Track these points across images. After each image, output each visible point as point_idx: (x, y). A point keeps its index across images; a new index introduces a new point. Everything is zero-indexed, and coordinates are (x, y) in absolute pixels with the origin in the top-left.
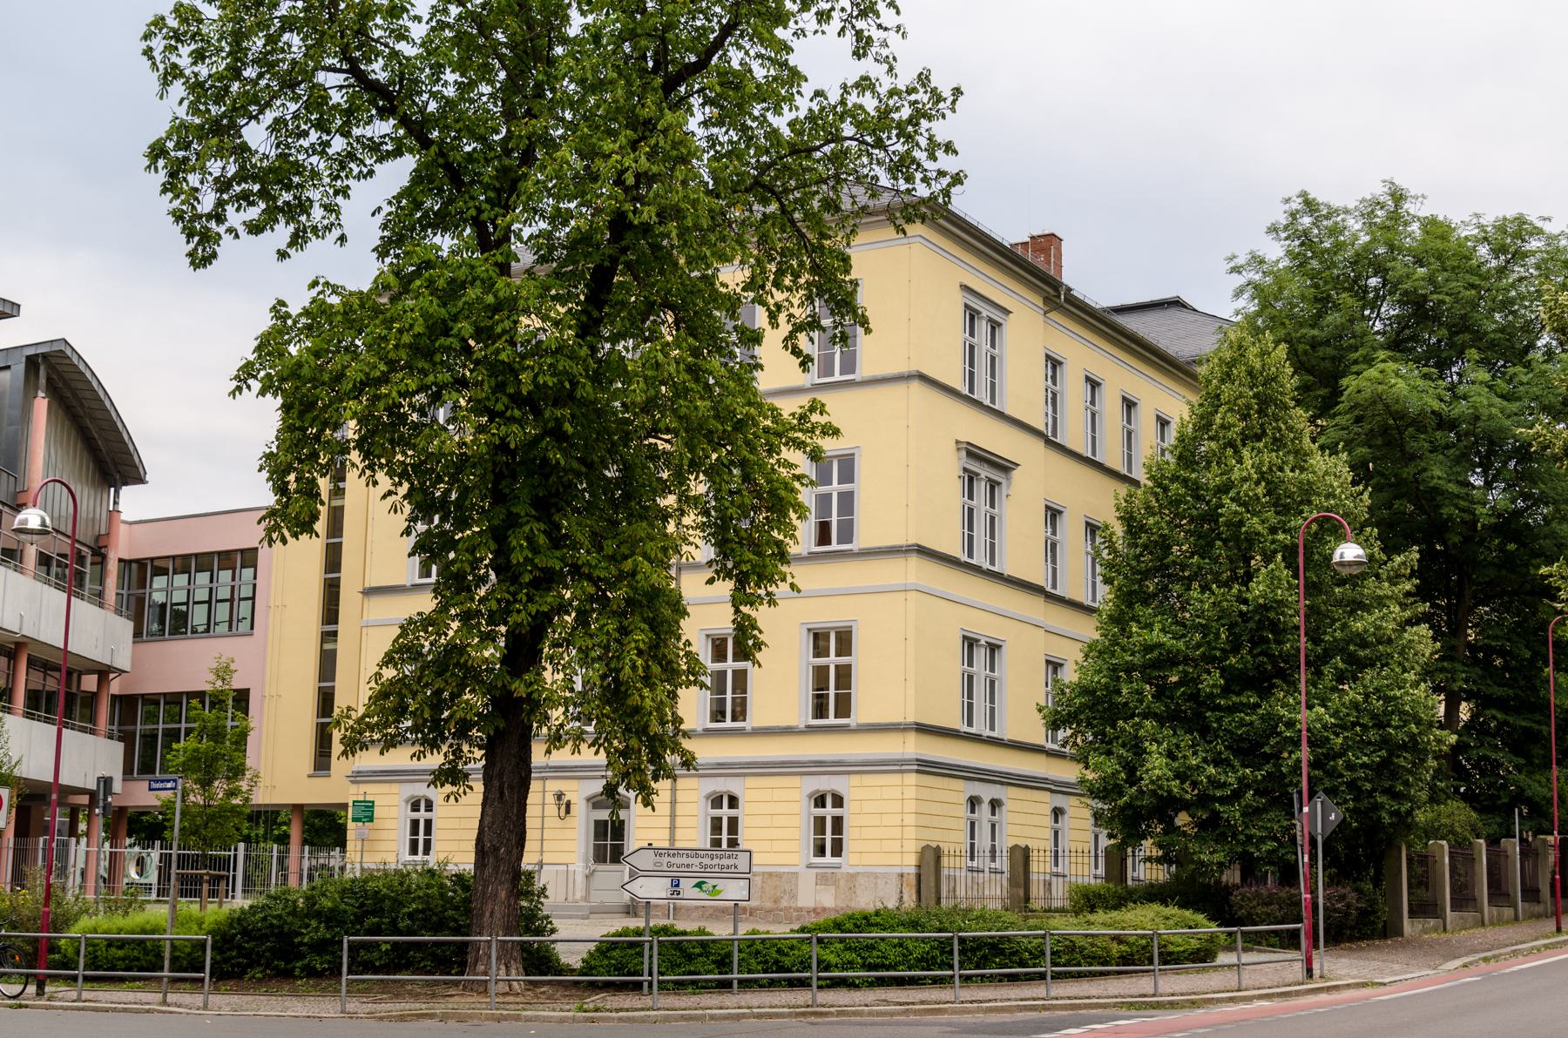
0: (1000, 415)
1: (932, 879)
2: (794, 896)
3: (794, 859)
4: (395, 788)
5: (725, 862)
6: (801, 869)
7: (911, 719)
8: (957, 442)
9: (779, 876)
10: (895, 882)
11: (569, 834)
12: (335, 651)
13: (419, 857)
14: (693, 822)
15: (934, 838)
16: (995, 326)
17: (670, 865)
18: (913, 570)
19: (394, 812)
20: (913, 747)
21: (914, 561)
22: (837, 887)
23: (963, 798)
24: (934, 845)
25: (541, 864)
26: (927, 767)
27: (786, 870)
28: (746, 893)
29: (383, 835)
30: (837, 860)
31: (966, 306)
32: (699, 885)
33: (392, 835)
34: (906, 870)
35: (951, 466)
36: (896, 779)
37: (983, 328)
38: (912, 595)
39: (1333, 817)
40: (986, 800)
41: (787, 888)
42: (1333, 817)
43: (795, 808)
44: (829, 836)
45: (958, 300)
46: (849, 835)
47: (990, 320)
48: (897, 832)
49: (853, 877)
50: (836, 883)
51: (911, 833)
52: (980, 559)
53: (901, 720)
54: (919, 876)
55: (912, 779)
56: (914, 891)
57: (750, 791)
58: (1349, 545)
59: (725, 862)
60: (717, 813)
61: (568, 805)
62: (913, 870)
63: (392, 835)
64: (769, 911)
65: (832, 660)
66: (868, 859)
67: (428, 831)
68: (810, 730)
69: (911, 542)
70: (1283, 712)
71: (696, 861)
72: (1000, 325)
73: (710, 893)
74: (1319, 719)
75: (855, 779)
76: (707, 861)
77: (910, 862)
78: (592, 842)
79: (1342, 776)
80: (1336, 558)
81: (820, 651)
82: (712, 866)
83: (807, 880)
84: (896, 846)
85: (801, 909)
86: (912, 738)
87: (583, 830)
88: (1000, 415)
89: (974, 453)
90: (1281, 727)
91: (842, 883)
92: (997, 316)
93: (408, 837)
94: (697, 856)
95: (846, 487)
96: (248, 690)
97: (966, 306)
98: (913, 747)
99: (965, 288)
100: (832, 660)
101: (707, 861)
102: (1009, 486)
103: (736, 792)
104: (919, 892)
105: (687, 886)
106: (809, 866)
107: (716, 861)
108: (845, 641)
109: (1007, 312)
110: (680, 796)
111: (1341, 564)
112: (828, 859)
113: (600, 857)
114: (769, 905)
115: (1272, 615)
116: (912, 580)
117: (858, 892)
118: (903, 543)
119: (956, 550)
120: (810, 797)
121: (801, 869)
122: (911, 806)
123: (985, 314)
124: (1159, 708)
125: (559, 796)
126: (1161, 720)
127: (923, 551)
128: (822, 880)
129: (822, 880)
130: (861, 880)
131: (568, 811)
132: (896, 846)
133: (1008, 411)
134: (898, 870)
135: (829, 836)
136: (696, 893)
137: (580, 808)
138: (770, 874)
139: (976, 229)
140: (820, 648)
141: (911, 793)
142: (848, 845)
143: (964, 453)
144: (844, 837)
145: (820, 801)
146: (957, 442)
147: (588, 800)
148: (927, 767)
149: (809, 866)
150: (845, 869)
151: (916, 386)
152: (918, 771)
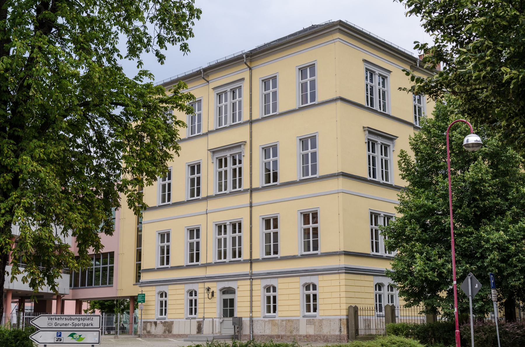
0: (388, 116)
1: (353, 321)
2: (298, 330)
3: (298, 313)
4: (182, 286)
5: (86, 322)
6: (301, 318)
7: (342, 249)
8: (364, 127)
9: (292, 321)
10: (338, 322)
11: (214, 305)
12: (141, 235)
13: (164, 316)
14: (258, 298)
15: (354, 302)
16: (384, 78)
17: (56, 324)
18: (340, 183)
19: (154, 298)
20: (342, 262)
21: (341, 179)
22: (315, 326)
23: (373, 285)
24: (354, 305)
25: (204, 318)
26: (349, 271)
27: (295, 318)
28: (97, 339)
29: (150, 308)
30: (315, 313)
31: (366, 69)
32: (72, 335)
33: (153, 307)
34: (342, 317)
35: (363, 138)
36: (336, 276)
37: (377, 79)
38: (341, 195)
39: (477, 286)
40: (386, 285)
41: (295, 326)
42: (477, 286)
43: (297, 291)
44: (311, 302)
45: (362, 67)
46: (319, 301)
47: (380, 75)
48: (338, 300)
49: (321, 321)
50: (314, 324)
51: (344, 300)
52: (379, 178)
53: (338, 250)
54: (347, 320)
55: (343, 276)
56: (346, 327)
57: (279, 283)
58: (472, 135)
59: (86, 322)
60: (268, 294)
61: (213, 293)
62: (345, 317)
63: (153, 307)
64: (288, 337)
65: (311, 225)
66: (327, 313)
67: (275, 302)
68: (303, 256)
69: (340, 171)
70: (484, 235)
71: (70, 322)
72: (386, 77)
73: (78, 339)
74: (501, 237)
75: (321, 277)
76: (76, 322)
77: (343, 314)
78: (222, 308)
79: (516, 266)
80: (465, 142)
81: (306, 222)
82: (79, 325)
83: (304, 321)
84: (338, 307)
85: (300, 336)
86: (343, 258)
87: (219, 303)
88: (388, 116)
89: (371, 132)
90: (483, 243)
91: (317, 324)
92: (384, 73)
93: (189, 307)
94: (71, 319)
95: (314, 150)
96: (114, 252)
97: (366, 69)
98: (342, 262)
99: (365, 61)
100: (311, 225)
101: (76, 322)
102: (394, 146)
103: (275, 285)
104: (348, 327)
105: (65, 336)
106: (304, 317)
107: (81, 322)
108: (315, 215)
109: (390, 72)
110: (254, 288)
111: (468, 145)
112: (272, 314)
113: (225, 315)
114: (288, 334)
115: (477, 187)
116: (340, 188)
117: (323, 327)
118: (336, 172)
119: (365, 174)
120: (303, 286)
121: (301, 318)
122: (343, 288)
123: (377, 72)
124: (426, 236)
125: (208, 289)
126: (424, 242)
127: (345, 175)
128: (309, 323)
129: (309, 323)
130: (324, 322)
131: (213, 295)
132: (338, 307)
133: (392, 114)
134: (339, 317)
135: (311, 302)
136: (70, 340)
137: (217, 294)
138: (289, 320)
139: (354, 28)
140: (306, 221)
141: (343, 282)
142: (319, 307)
143: (367, 132)
144: (277, 304)
145: (307, 288)
146: (364, 127)
147: (220, 290)
148: (349, 271)
149: (304, 317)
150: (318, 318)
151: (339, 103)
152: (346, 273)
